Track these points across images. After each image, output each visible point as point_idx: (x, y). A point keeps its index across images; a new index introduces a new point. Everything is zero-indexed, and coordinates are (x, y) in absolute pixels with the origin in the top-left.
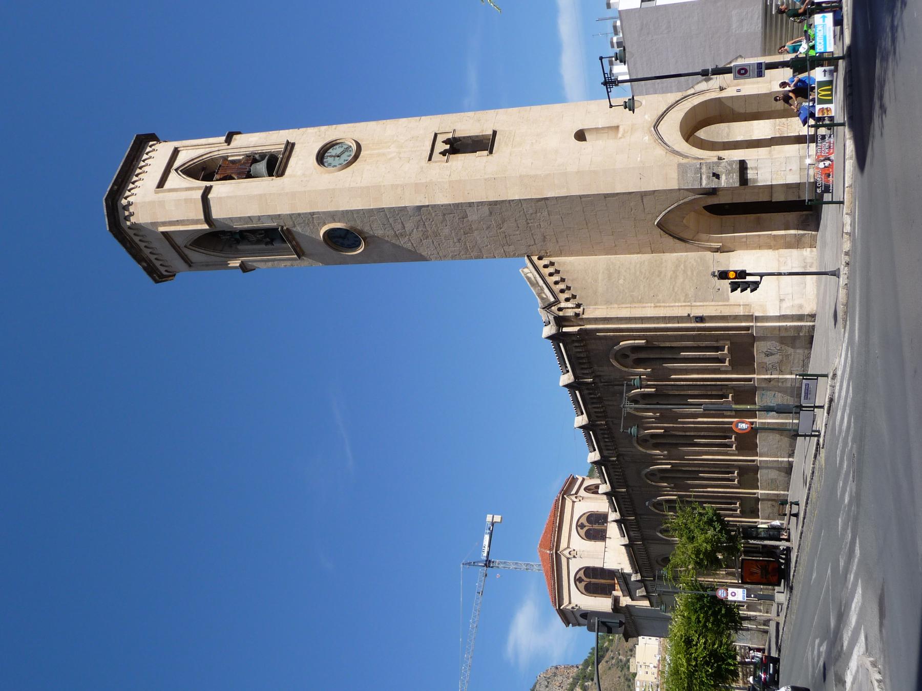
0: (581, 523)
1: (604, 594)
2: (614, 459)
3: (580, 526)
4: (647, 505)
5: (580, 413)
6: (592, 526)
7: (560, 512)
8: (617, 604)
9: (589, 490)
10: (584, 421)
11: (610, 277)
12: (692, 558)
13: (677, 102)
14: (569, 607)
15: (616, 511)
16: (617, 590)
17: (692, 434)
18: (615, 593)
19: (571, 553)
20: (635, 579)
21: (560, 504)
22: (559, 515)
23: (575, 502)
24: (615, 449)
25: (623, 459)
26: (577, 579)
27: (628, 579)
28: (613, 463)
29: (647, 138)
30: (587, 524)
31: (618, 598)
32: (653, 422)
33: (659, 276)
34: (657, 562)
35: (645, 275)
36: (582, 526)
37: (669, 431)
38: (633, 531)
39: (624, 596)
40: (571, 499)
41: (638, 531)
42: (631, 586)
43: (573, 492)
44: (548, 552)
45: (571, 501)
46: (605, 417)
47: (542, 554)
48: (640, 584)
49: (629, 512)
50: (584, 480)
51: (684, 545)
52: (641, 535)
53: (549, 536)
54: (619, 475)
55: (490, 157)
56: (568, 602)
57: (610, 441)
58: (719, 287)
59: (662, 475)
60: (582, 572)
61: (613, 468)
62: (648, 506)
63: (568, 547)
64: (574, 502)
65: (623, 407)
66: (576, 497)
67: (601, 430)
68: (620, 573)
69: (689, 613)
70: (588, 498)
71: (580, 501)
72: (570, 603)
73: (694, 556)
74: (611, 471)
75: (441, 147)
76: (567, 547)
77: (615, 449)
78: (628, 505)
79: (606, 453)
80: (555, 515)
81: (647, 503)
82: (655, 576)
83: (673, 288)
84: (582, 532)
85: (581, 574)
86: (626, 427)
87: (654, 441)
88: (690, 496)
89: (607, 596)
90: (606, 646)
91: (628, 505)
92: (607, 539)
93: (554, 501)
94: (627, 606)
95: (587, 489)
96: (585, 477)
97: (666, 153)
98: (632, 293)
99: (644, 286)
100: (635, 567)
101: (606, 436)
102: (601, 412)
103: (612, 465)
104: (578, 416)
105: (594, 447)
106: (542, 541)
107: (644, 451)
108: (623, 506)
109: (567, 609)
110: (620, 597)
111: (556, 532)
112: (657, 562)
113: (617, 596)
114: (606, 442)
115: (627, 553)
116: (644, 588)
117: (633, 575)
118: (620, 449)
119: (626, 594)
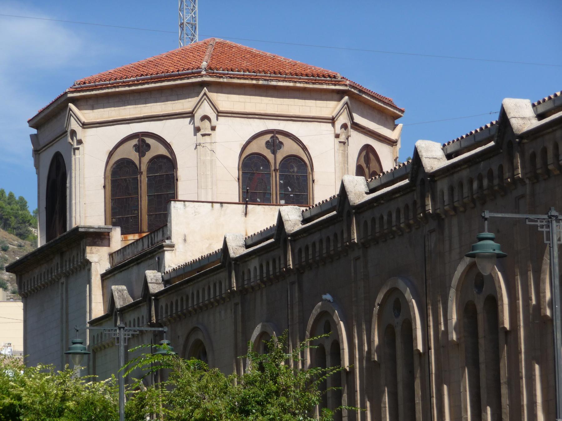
0: (281, 143)
1: (113, 209)
2: (430, 208)
4: (324, 297)
5: (541, 109)
7: (305, 89)
8: (90, 240)
9: (367, 160)
10: (521, 122)
12: (192, 411)
14: (74, 125)
15: (305, 221)
16: (125, 240)
17: (505, 401)
18: (116, 235)
19: (206, 121)
20: (149, 280)
21: (325, 87)
22: (298, 85)
23: (333, 125)
24: (455, 209)
25: (431, 232)
26: (144, 141)
27: (151, 262)
28: (419, 205)
30: (280, 156)
31: (105, 242)
32: (527, 299)
34: (195, 329)
37: (506, 343)
38: (261, 266)
39: (111, 255)
40: (339, 114)
41: (262, 279)
42: (134, 271)
43: (358, 119)
44: (204, 64)
45: (334, 114)
46: (535, 178)
47: (199, 51)
48: (139, 292)
49: (303, 255)
50: (392, 143)
51: (224, 390)
52: (253, 288)
53: (245, 64)
54: (390, 222)
56: (86, 121)
57: (472, 195)
59: (398, 330)
60: (162, 151)
61: (407, 207)
62: (322, 300)
63: (220, 114)
64: (332, 121)
65: (550, 217)
66: (345, 126)
67: (501, 168)
68: (163, 241)
69: (71, 411)
70: (346, 156)
71: (337, 136)
72: (85, 125)
73: (198, 416)
74: (400, 202)
76: (221, 109)
77: (455, 209)
78: (321, 249)
79: (443, 185)
80: (296, 75)
81: (328, 297)
82: (162, 327)
84: (259, 147)
85: (157, 149)
86: (495, 225)
87: (480, 307)
88: (352, 402)
89: (109, 215)
90: (30, 232)
91: (321, 249)
92: (242, 207)
93: (331, 72)
94: (88, 264)
95: (368, 150)
96: (399, 145)
100: (178, 277)
101: (485, 182)
102: (545, 164)
103: (415, 203)
104: (534, 105)
105: (457, 154)
106: (231, 47)
107: (455, 282)
108: (316, 237)
109: (69, 120)
110: (109, 246)
111: (254, 82)
112: (195, 329)
113: (109, 240)
114: (471, 182)
115: (210, 256)
116: (132, 301)
117: (159, 275)
118: (455, 221)
119: (118, 260)
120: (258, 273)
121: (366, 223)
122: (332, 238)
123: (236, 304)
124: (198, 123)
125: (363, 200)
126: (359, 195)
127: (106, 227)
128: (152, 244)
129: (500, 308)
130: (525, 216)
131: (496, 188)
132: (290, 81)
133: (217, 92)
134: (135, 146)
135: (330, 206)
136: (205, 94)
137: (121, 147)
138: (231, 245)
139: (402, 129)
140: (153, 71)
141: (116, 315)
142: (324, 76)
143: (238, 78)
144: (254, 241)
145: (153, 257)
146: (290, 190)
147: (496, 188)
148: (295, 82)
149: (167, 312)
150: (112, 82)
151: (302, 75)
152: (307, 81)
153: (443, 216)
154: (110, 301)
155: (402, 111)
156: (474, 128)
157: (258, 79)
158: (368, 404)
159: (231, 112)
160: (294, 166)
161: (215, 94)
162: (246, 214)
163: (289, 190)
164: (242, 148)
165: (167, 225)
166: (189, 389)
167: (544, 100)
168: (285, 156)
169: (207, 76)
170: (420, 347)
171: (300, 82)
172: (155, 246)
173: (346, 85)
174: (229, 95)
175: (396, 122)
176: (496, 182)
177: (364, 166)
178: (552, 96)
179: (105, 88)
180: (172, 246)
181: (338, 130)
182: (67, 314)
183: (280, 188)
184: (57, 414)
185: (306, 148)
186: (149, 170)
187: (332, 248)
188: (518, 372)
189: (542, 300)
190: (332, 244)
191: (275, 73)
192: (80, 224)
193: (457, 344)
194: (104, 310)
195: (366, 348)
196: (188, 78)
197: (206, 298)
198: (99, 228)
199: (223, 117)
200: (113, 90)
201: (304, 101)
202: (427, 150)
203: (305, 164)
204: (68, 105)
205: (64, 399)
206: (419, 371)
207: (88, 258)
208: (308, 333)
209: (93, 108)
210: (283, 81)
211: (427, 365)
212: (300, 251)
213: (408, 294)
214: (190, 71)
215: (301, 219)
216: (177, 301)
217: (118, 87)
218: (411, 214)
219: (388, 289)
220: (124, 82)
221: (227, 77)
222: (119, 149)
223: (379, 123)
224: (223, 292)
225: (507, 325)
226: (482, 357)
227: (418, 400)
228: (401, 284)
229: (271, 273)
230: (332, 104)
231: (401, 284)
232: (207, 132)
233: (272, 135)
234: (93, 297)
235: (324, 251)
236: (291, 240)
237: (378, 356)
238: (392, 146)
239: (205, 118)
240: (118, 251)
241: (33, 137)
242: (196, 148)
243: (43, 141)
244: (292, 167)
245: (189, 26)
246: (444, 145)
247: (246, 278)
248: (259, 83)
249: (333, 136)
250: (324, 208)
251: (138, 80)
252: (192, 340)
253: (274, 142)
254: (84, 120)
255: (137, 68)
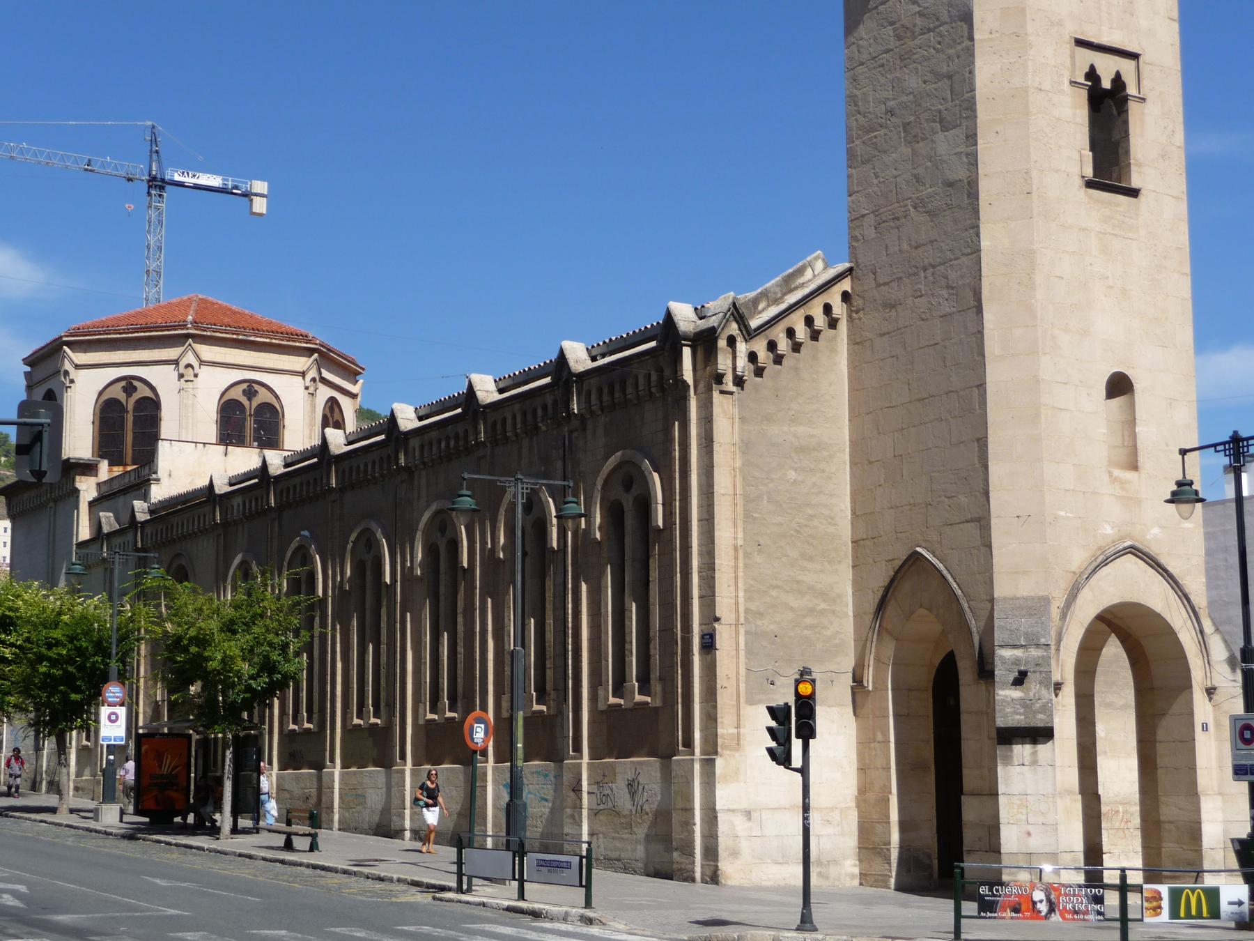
0: (256, 392)
2: (402, 462)
3: (251, 389)
4: (302, 533)
5: (502, 385)
7: (279, 345)
9: (332, 410)
10: (485, 394)
11: (802, 450)
12: (188, 629)
13: (1185, 597)
14: (67, 366)
15: (286, 466)
16: (110, 471)
17: (460, 628)
18: (104, 466)
20: (136, 509)
21: (298, 344)
22: (274, 341)
24: (424, 463)
26: (131, 383)
27: (138, 492)
28: (393, 458)
29: (1108, 530)
30: (255, 403)
31: (94, 472)
32: (483, 543)
33: (803, 556)
35: (806, 526)
36: (250, 393)
38: (244, 503)
39: (99, 485)
40: (309, 369)
42: (120, 501)
43: (326, 374)
44: (190, 318)
45: (305, 369)
47: (185, 305)
48: (126, 519)
49: (285, 495)
50: (353, 396)
52: (235, 521)
53: (226, 320)
54: (366, 471)
55: (1079, 182)
56: (79, 363)
57: (440, 452)
58: (777, 683)
60: (148, 393)
61: (382, 459)
62: (300, 535)
63: (202, 363)
64: (303, 374)
65: (516, 480)
66: (314, 380)
67: (466, 431)
68: (149, 475)
69: (65, 623)
70: (313, 406)
71: (307, 388)
72: (77, 367)
75: (1107, 68)
76: (204, 358)
77: (424, 463)
79: (414, 443)
80: (272, 332)
81: (306, 533)
82: (147, 552)
83: (777, 587)
84: (237, 394)
85: (144, 391)
86: (472, 484)
87: (442, 548)
88: (323, 624)
92: (222, 448)
93: (304, 331)
94: (77, 491)
95: (333, 404)
97: (1074, 573)
98: (765, 498)
99: (780, 524)
101: (452, 443)
102: (505, 431)
103: (389, 457)
104: (495, 381)
106: (213, 304)
107: (421, 526)
108: (297, 480)
111: (235, 336)
112: (178, 555)
113: (97, 470)
114: (439, 442)
117: (145, 505)
118: (424, 473)
119: (104, 489)
120: (241, 508)
121: (344, 472)
122: (312, 482)
123: (219, 535)
124: (182, 370)
125: (342, 451)
126: (339, 447)
127: (94, 459)
128: (139, 477)
129: (460, 549)
130: (496, 478)
131: (461, 448)
132: (266, 338)
134: (123, 387)
135: (310, 454)
136: (190, 345)
137: (110, 388)
138: (217, 484)
139: (363, 384)
140: (142, 321)
141: (102, 539)
142: (297, 335)
144: (238, 480)
145: (139, 489)
147: (461, 448)
149: (152, 539)
150: (104, 329)
151: (277, 332)
153: (414, 469)
154: (97, 526)
155: (363, 369)
156: (444, 396)
157: (238, 334)
158: (338, 627)
162: (226, 455)
165: (153, 461)
166: (186, 611)
167: (505, 378)
168: (259, 403)
170: (388, 580)
172: (142, 479)
175: (357, 378)
176: (461, 443)
177: (329, 415)
178: (512, 375)
179: (98, 335)
180: (158, 480)
181: (308, 383)
182: (54, 536)
183: (254, 432)
184: (54, 626)
186: (136, 409)
187: (311, 491)
188: (473, 604)
189: (497, 545)
190: (311, 487)
191: (253, 329)
193: (421, 579)
194: (90, 534)
195: (339, 579)
196: (175, 330)
197: (191, 528)
198: (88, 460)
200: (106, 336)
202: (402, 412)
203: (277, 410)
204: (62, 348)
205: (60, 613)
206: (385, 600)
207: (77, 486)
208: (285, 564)
209: (85, 351)
210: (260, 337)
211: (393, 596)
212: (282, 491)
213: (379, 535)
214: (177, 324)
215: (283, 464)
216: (162, 529)
217: (110, 334)
218: (385, 465)
219: (361, 528)
220: (115, 330)
222: (107, 390)
223: (343, 378)
224: (207, 523)
225: (465, 564)
226: (442, 589)
227: (383, 625)
228: (373, 525)
229: (253, 509)
230: (303, 359)
231: (373, 525)
234: (80, 521)
235: (304, 493)
236: (273, 482)
237: (349, 586)
238: (353, 398)
239: (189, 366)
240: (105, 482)
241: (26, 373)
242: (179, 392)
243: (35, 379)
245: (155, 274)
246: (416, 409)
247: (229, 512)
249: (303, 388)
250: (304, 456)
251: (128, 329)
252: (174, 566)
253: (250, 390)
254: (77, 362)
255: (127, 317)
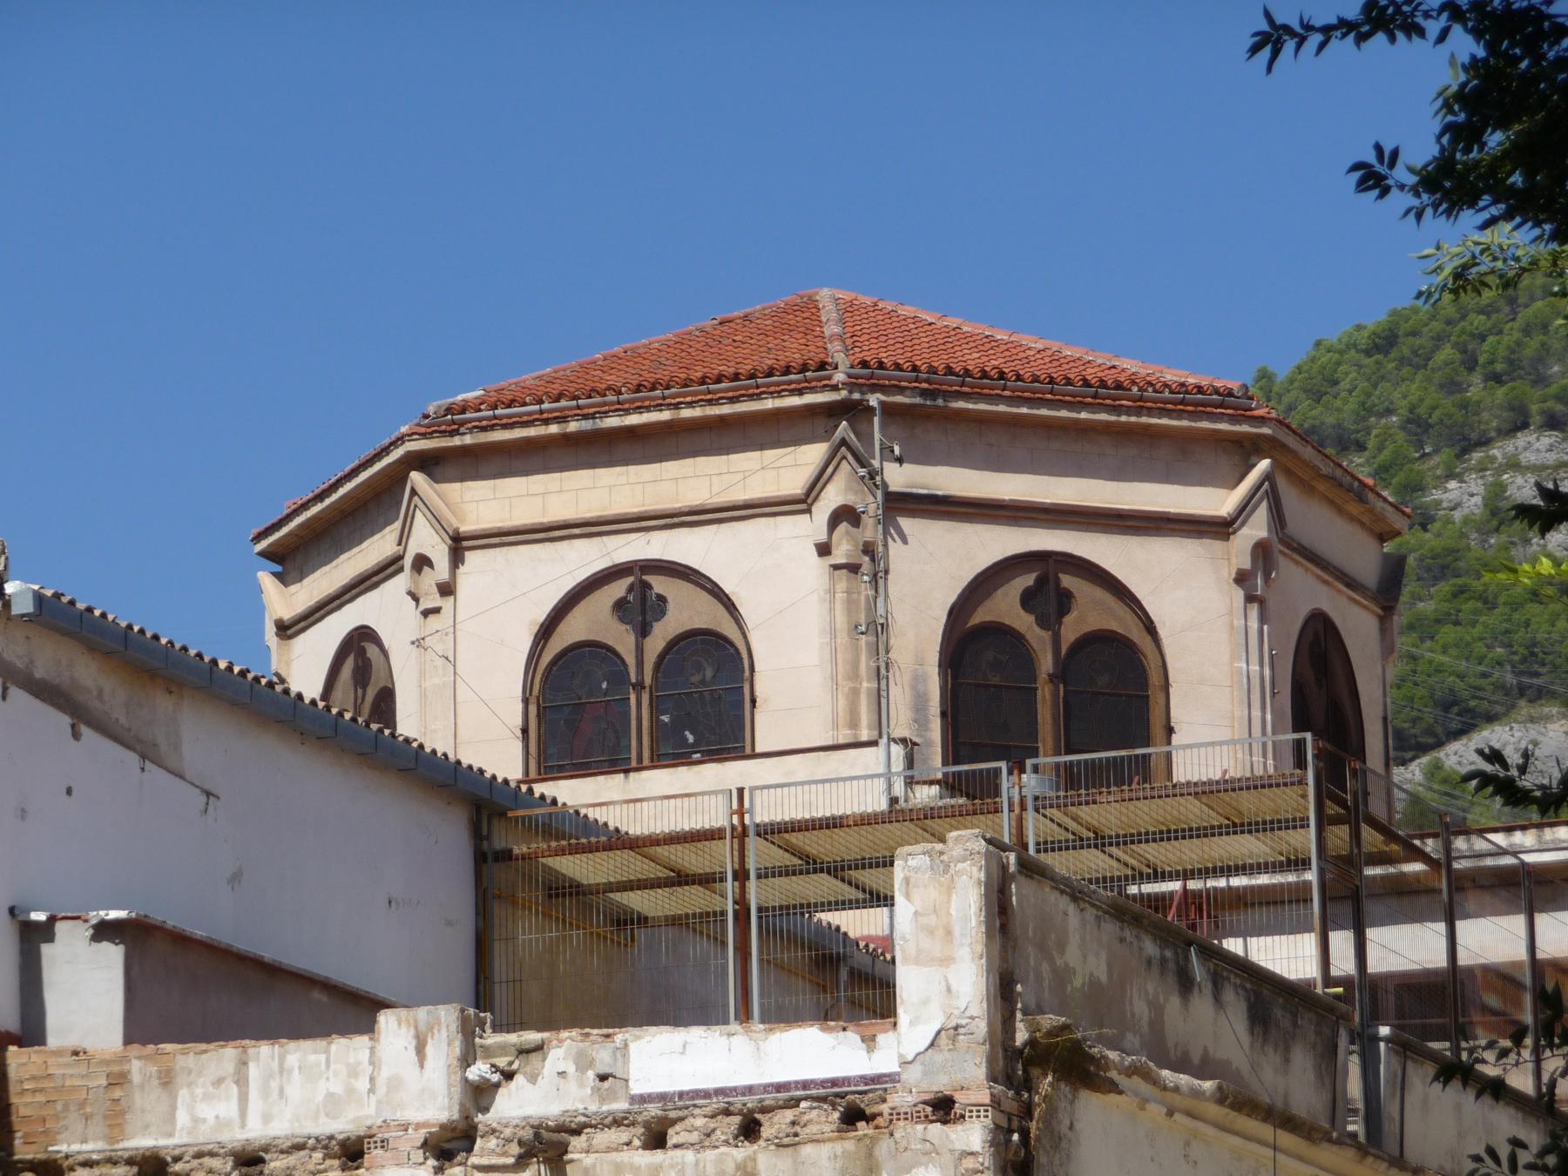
0: (662, 599)
6: (639, 686)
21: (769, 404)
22: (686, 413)
30: (656, 642)
110: (869, 1041)
111: (554, 429)
132: (659, 407)
133: (462, 480)
143: (505, 427)
146: (691, 738)
148: (676, 406)
152: (730, 394)
157: (562, 420)
159: (496, 531)
160: (705, 664)
161: (457, 486)
163: (687, 740)
164: (536, 636)
169: (414, 437)
171: (690, 405)
173: (835, 388)
174: (498, 481)
185: (733, 604)
186: (1061, 675)
192: (1232, 742)
199: (479, 552)
201: (725, 457)
204: (405, 478)
221: (471, 430)
232: (430, 605)
233: (630, 580)
244: (699, 668)
248: (568, 430)
